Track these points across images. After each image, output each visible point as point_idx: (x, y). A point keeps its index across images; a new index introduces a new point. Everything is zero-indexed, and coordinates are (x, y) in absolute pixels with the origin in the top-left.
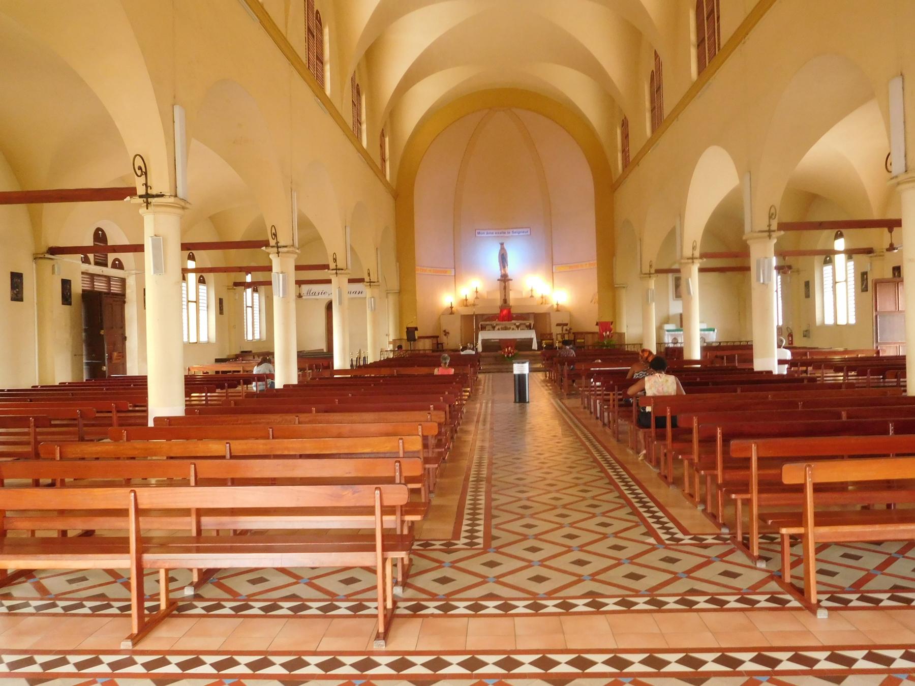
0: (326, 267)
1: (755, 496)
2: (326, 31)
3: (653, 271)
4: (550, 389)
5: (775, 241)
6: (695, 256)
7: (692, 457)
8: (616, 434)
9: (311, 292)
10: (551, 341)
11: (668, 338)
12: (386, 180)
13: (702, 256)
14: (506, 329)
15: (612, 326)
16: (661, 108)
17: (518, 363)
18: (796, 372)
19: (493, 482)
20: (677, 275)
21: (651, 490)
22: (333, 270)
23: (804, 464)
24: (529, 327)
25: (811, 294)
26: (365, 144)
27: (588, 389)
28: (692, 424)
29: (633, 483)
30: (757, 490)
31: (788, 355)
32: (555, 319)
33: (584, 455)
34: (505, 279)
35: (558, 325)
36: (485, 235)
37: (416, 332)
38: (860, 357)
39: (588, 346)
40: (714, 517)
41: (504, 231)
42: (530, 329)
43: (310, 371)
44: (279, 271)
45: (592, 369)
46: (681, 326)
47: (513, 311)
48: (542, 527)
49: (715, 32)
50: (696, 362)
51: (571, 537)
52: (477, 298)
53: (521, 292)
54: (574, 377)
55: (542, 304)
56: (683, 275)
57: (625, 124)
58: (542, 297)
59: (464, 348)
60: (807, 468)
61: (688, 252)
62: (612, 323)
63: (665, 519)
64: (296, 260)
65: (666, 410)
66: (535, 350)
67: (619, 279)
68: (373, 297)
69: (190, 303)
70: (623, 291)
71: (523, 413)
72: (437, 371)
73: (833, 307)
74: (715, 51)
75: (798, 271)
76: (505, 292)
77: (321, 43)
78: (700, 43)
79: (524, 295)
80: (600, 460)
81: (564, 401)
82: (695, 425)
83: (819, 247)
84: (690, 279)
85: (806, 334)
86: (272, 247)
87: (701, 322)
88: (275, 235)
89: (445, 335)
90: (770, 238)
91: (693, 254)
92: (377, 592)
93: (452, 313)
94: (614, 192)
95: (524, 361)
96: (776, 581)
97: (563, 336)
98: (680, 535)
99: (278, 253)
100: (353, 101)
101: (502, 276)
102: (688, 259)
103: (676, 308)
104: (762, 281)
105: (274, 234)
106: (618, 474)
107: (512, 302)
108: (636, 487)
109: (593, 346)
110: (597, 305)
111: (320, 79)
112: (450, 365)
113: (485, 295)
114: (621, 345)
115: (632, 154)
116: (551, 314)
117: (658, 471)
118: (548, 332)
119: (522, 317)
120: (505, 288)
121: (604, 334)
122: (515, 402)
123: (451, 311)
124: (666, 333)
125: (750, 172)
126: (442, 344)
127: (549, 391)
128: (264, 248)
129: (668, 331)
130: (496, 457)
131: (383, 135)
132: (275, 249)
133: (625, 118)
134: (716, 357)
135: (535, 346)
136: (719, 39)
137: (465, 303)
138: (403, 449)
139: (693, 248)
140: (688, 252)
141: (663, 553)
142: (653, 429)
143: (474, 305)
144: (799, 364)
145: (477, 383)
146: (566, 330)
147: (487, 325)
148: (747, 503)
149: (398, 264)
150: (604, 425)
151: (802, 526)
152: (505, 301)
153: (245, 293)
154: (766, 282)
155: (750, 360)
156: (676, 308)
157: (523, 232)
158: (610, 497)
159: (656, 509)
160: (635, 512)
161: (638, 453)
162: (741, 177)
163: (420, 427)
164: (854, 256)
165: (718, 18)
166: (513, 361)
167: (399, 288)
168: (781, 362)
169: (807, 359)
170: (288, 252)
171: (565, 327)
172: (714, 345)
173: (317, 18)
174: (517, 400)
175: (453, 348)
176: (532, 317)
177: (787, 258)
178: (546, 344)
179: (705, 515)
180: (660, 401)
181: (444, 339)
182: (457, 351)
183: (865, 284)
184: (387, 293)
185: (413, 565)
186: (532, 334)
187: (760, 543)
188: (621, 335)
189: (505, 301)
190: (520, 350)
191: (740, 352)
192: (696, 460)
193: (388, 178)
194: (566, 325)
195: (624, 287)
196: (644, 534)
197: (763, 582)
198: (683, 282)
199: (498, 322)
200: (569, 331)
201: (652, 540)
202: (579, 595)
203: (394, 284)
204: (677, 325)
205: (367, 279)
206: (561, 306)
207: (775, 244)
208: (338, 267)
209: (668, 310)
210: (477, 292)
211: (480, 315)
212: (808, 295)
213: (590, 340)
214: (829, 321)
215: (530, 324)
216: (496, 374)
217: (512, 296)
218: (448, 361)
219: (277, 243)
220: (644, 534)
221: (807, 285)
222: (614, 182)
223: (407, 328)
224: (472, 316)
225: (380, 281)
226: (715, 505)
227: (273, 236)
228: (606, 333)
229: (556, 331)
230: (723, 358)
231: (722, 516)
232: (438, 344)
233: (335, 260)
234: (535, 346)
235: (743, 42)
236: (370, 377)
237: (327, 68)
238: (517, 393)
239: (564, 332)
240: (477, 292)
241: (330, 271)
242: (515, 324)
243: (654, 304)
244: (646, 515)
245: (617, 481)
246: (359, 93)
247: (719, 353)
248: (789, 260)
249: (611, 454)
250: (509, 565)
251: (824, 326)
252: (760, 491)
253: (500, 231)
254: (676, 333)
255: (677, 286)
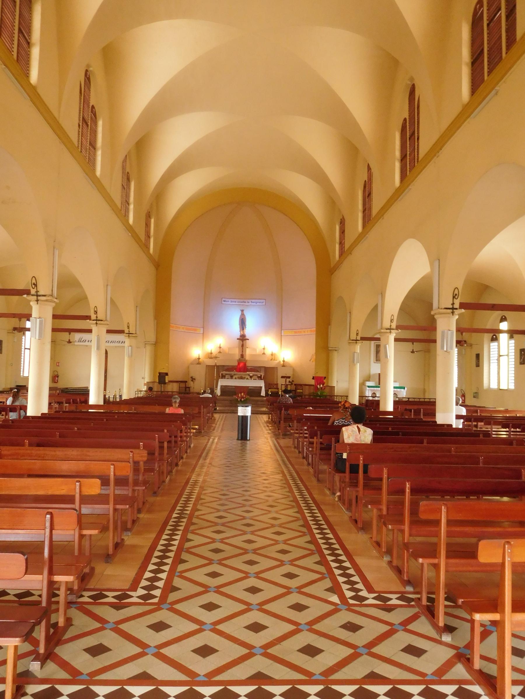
0: (88, 318)
1: (443, 561)
2: (100, 123)
3: (359, 338)
4: (270, 430)
5: (457, 317)
6: (392, 327)
7: (381, 507)
8: (317, 473)
9: (82, 340)
10: (277, 390)
11: (369, 392)
12: (150, 253)
13: (398, 328)
14: (241, 378)
15: (325, 381)
16: (370, 209)
17: (243, 406)
18: (469, 426)
19: (195, 520)
20: (377, 342)
21: (341, 535)
22: (93, 320)
23: (503, 541)
24: (260, 378)
25: (480, 364)
26: (131, 221)
27: (298, 432)
28: (382, 475)
29: (325, 526)
30: (445, 556)
31: (463, 411)
32: (281, 372)
33: (286, 493)
34: (243, 338)
35: (282, 377)
36: (230, 303)
37: (166, 376)
38: (519, 417)
39: (305, 395)
40: (399, 571)
41: (245, 301)
42: (261, 379)
43: (67, 405)
44: (37, 316)
45: (304, 415)
46: (379, 384)
47: (248, 364)
48: (260, 542)
49: (415, 149)
50: (389, 413)
51: (284, 552)
52: (220, 352)
53: (255, 350)
54: (288, 419)
55: (271, 360)
56: (382, 343)
57: (342, 223)
58: (272, 355)
59: (205, 392)
60: (507, 546)
61: (387, 324)
62: (325, 378)
63: (351, 571)
64: (54, 309)
65: (359, 458)
66: (263, 397)
67: (332, 344)
68: (131, 346)
69: (26, 350)
70: (335, 353)
71: (243, 449)
72: (168, 410)
73: (497, 375)
74: (415, 164)
75: (471, 345)
76: (243, 349)
77: (94, 133)
78: (403, 158)
79: (258, 352)
80: (299, 499)
81: (279, 441)
82: (385, 476)
83: (488, 327)
84: (387, 345)
85: (476, 395)
86: (32, 295)
87: (395, 381)
88: (36, 285)
89: (192, 381)
90: (453, 315)
91: (391, 326)
92: (6, 668)
93: (199, 363)
94: (332, 274)
95: (246, 405)
96: (463, 664)
97: (286, 386)
98: (364, 593)
99: (37, 301)
100: (122, 185)
101: (241, 336)
102: (387, 329)
103: (375, 369)
104: (445, 349)
105: (34, 284)
106: (313, 517)
107: (247, 357)
108: (328, 531)
109: (310, 395)
110: (314, 363)
111: (92, 162)
112: (179, 406)
113: (227, 351)
114: (331, 396)
115: (347, 244)
116: (278, 369)
117: (350, 514)
118: (275, 383)
119: (255, 369)
120: (243, 346)
121: (319, 386)
122: (238, 439)
123: (198, 362)
124: (368, 388)
125: (439, 260)
126: (189, 388)
127: (269, 432)
128: (25, 296)
129: (369, 387)
130: (206, 492)
131: (148, 216)
132: (35, 297)
133: (343, 217)
134: (406, 410)
135: (263, 393)
136: (418, 154)
137: (210, 356)
138: (80, 491)
139: (391, 321)
140: (387, 324)
141: (345, 616)
142: (347, 474)
143: (216, 357)
144: (473, 419)
145: (211, 420)
146: (290, 382)
147: (226, 374)
148: (436, 566)
149: (156, 321)
150: (309, 464)
151: (497, 612)
152: (242, 356)
153: (23, 337)
154: (449, 350)
155: (433, 414)
156: (375, 369)
157: (260, 303)
158: (301, 541)
159: (343, 558)
160: (323, 562)
161: (334, 494)
162: (432, 264)
163: (112, 467)
164: (515, 336)
165: (418, 139)
166: (238, 405)
167: (155, 340)
168: (458, 417)
169: (478, 416)
170: (47, 301)
171: (288, 380)
172: (404, 400)
173: (92, 112)
174: (240, 439)
175: (197, 391)
176: (263, 369)
177: (464, 333)
178: (271, 392)
179: (390, 568)
180: (355, 447)
181: (191, 384)
182: (199, 394)
183: (523, 358)
184: (145, 344)
185: (72, 625)
186: (261, 384)
187: (446, 606)
188: (333, 388)
189: (242, 356)
190: (251, 396)
191: (425, 407)
192: (385, 512)
193: (151, 251)
194: (289, 377)
195: (336, 350)
196: (328, 590)
197: (448, 665)
198: (382, 349)
199: (236, 373)
200: (291, 383)
201: (335, 599)
202: (244, 678)
203: (152, 337)
204: (376, 383)
205: (127, 331)
206: (287, 362)
207: (457, 320)
208: (98, 318)
209: (370, 371)
210: (220, 347)
211: (221, 366)
212: (478, 365)
213: (307, 391)
214: (494, 385)
215: (261, 376)
216: (229, 415)
217: (248, 352)
218: (178, 401)
219: (37, 292)
220: (328, 590)
221: (478, 356)
222: (332, 266)
223: (160, 373)
224: (214, 366)
225: (138, 332)
226: (401, 557)
227: (33, 286)
228: (320, 386)
229: (281, 382)
230: (410, 411)
231: (407, 572)
232: (186, 388)
233: (96, 312)
234: (263, 393)
235: (437, 155)
236: (123, 413)
237: (99, 153)
238: (240, 431)
239: (288, 383)
240: (220, 347)
241: (91, 322)
242: (249, 375)
243: (358, 364)
244: (334, 565)
245: (311, 523)
246: (128, 179)
247: (408, 407)
248: (466, 336)
249: (310, 494)
250: (229, 575)
251: (489, 390)
252: (448, 557)
253: (242, 301)
254: (375, 389)
255: (378, 352)
